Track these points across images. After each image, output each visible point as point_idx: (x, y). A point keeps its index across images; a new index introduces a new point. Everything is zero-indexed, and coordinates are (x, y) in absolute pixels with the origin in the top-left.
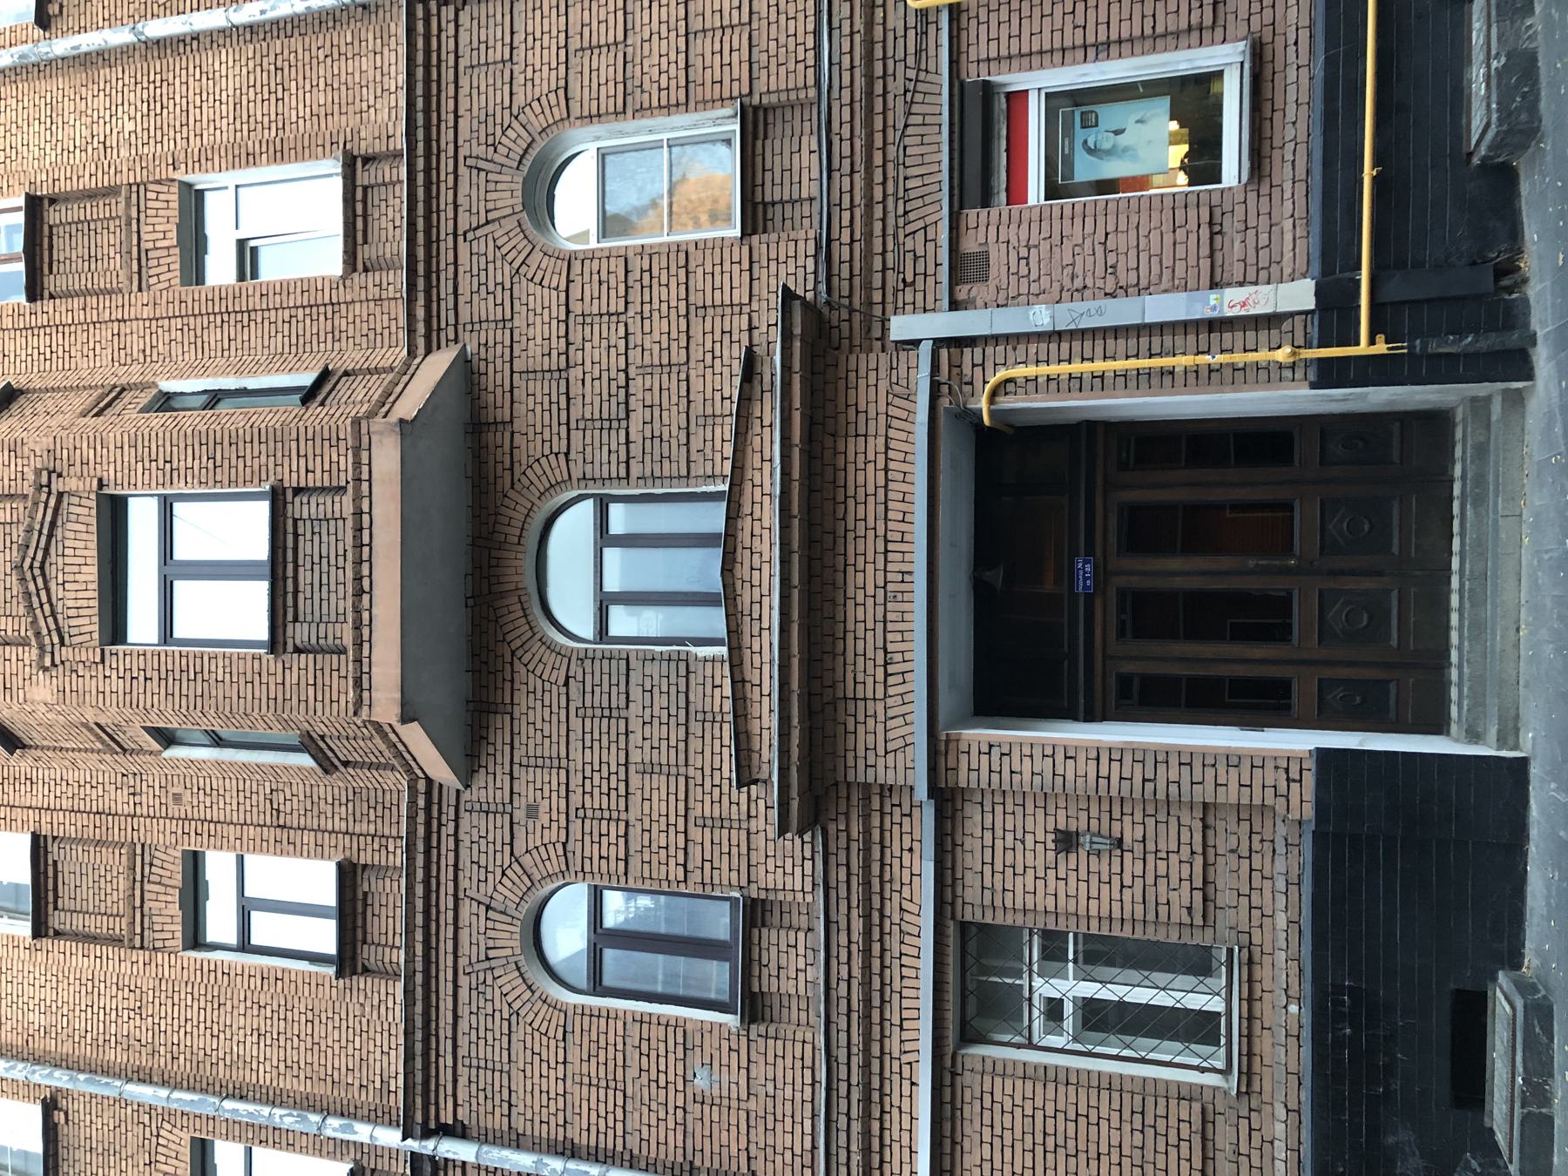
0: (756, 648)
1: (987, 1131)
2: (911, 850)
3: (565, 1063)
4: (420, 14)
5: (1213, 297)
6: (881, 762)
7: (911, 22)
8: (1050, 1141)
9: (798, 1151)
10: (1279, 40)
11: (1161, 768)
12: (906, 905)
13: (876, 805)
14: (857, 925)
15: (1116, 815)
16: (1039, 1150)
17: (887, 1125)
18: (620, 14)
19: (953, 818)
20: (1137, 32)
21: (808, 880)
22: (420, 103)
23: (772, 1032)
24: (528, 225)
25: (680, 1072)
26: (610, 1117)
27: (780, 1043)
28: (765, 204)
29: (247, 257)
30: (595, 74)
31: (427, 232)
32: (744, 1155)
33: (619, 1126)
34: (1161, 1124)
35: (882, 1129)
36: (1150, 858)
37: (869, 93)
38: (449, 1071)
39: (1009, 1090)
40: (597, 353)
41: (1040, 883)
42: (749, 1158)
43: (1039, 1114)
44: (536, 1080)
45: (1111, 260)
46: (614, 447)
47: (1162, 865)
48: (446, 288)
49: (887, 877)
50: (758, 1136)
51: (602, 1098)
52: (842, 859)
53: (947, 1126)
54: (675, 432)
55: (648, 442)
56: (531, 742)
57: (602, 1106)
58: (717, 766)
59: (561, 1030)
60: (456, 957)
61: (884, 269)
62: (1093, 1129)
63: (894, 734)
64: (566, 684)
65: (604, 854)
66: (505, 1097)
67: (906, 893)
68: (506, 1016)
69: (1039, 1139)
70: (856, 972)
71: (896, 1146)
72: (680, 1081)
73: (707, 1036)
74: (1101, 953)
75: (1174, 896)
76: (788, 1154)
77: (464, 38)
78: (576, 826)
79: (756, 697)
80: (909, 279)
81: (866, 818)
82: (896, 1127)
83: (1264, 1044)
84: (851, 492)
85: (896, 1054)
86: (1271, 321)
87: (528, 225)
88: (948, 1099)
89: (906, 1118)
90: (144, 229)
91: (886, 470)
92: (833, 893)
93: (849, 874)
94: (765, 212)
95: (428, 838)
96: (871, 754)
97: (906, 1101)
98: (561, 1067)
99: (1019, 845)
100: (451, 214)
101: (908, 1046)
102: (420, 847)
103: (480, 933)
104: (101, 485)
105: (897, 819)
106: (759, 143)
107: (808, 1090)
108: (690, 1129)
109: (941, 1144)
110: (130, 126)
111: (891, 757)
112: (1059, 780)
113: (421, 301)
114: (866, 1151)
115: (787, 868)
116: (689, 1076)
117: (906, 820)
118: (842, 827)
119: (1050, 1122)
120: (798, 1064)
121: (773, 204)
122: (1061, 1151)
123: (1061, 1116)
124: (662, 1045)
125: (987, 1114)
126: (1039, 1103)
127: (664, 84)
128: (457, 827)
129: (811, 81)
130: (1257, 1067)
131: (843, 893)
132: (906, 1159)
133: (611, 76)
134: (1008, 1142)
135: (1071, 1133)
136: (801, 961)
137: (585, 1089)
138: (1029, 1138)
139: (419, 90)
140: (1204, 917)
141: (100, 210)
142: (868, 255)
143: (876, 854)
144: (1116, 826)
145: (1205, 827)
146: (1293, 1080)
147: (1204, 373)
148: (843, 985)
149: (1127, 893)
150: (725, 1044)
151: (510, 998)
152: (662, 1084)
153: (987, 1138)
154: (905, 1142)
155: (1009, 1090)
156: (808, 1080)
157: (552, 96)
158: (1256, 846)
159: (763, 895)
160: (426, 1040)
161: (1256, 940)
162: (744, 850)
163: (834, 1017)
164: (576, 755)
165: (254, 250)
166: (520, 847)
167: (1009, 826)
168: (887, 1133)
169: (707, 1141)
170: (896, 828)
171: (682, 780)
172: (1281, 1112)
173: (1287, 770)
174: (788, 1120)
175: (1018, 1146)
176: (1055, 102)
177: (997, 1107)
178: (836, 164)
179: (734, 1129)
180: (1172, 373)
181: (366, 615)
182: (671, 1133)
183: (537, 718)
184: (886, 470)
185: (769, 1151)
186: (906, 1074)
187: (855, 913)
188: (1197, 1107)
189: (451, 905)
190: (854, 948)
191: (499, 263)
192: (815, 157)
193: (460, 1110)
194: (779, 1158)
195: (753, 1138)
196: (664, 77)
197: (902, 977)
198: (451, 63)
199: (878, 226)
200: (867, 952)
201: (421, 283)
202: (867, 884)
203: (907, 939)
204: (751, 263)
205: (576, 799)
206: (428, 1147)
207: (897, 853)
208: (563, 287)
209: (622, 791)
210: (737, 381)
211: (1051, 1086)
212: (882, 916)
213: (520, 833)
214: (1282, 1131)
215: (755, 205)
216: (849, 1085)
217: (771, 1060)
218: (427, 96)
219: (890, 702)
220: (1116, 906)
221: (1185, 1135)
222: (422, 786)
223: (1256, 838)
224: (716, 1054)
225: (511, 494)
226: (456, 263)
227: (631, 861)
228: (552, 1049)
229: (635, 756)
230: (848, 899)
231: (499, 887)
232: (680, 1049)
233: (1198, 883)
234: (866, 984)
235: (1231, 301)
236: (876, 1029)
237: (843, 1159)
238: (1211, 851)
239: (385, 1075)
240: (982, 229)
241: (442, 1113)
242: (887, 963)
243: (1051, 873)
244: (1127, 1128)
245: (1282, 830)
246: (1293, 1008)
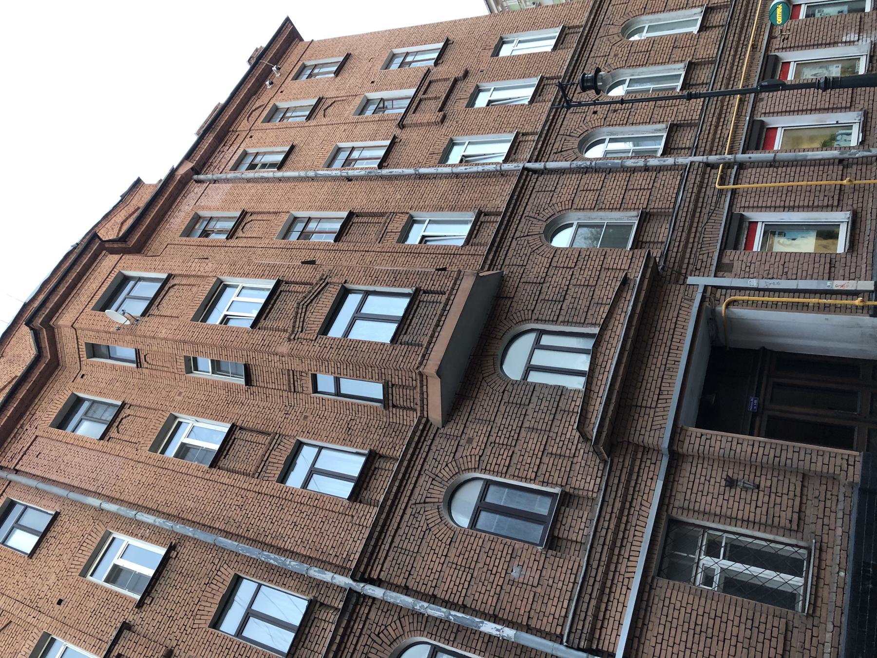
0: (600, 378)
1: (664, 618)
2: (652, 479)
3: (446, 556)
5: (829, 283)
6: (647, 434)
7: (716, 193)
8: (698, 628)
9: (557, 616)
10: (864, 213)
11: (784, 453)
12: (644, 503)
13: (639, 456)
14: (618, 505)
15: (758, 474)
16: (691, 632)
17: (609, 608)
19: (676, 468)
20: (806, 204)
21: (597, 486)
25: (505, 568)
26: (461, 586)
27: (562, 560)
31: (503, 235)
32: (526, 615)
33: (464, 591)
34: (762, 627)
35: (606, 609)
36: (773, 496)
37: (695, 211)
38: (385, 552)
39: (680, 598)
40: (558, 279)
41: (714, 501)
42: (529, 618)
43: (694, 613)
44: (428, 563)
45: (786, 270)
47: (778, 500)
49: (637, 489)
50: (537, 606)
51: (460, 576)
52: (618, 474)
53: (642, 613)
56: (479, 412)
57: (458, 580)
58: (565, 432)
59: (450, 540)
60: (409, 500)
61: (688, 264)
62: (723, 625)
63: (658, 425)
64: (503, 392)
65: (498, 462)
66: (409, 569)
67: (645, 497)
68: (424, 529)
69: (692, 626)
70: (612, 526)
71: (612, 620)
72: (504, 572)
73: (525, 551)
74: (737, 553)
75: (783, 514)
76: (551, 617)
78: (489, 449)
80: (698, 267)
81: (634, 460)
82: (614, 609)
83: (824, 592)
84: (658, 329)
85: (622, 572)
86: (855, 294)
88: (645, 599)
89: (620, 605)
91: (676, 323)
92: (609, 489)
93: (619, 481)
95: (417, 443)
96: (643, 430)
97: (622, 597)
98: (443, 558)
99: (707, 483)
101: (630, 569)
102: (413, 445)
103: (428, 488)
104: (345, 282)
105: (648, 464)
107: (571, 585)
108: (501, 598)
109: (636, 622)
110: (399, 197)
111: (652, 432)
112: (732, 452)
113: (492, 254)
114: (596, 617)
115: (588, 478)
116: (509, 571)
117: (652, 466)
118: (621, 460)
119: (700, 618)
120: (569, 572)
122: (703, 634)
123: (706, 615)
124: (500, 553)
125: (665, 609)
126: (695, 607)
128: (431, 443)
129: (672, 206)
130: (819, 603)
131: (614, 489)
132: (616, 627)
134: (674, 625)
135: (711, 625)
136: (583, 525)
137: (452, 570)
138: (686, 625)
139: (517, 193)
140: (798, 526)
142: (683, 257)
143: (634, 477)
144: (757, 479)
145: (803, 486)
146: (839, 610)
147: (822, 307)
148: (604, 531)
149: (758, 510)
150: (533, 557)
151: (429, 522)
152: (494, 572)
153: (663, 622)
154: (617, 618)
155: (680, 598)
156: (572, 580)
158: (829, 496)
159: (572, 491)
160: (380, 533)
161: (825, 540)
162: (568, 469)
163: (595, 546)
164: (498, 420)
166: (458, 455)
167: (704, 473)
168: (608, 612)
169: (509, 604)
170: (647, 469)
172: (830, 627)
173: (847, 460)
174: (556, 599)
175: (680, 628)
176: (768, 228)
177: (672, 606)
178: (677, 228)
179: (525, 600)
180: (808, 306)
181: (437, 334)
182: (491, 598)
183: (486, 403)
184: (676, 323)
185: (541, 614)
186: (626, 582)
187: (618, 499)
188: (783, 621)
189: (416, 475)
190: (614, 515)
192: (667, 230)
193: (382, 573)
194: (545, 619)
195: (534, 607)
197: (634, 536)
199: (689, 250)
200: (619, 519)
201: (494, 249)
202: (627, 489)
203: (641, 518)
205: (492, 439)
206: (359, 587)
207: (645, 479)
209: (515, 438)
210: (618, 284)
211: (703, 600)
212: (631, 506)
213: (461, 449)
214: (830, 634)
215: (638, 241)
216: (595, 581)
217: (555, 568)
219: (657, 410)
220: (752, 515)
221: (775, 635)
222: (424, 420)
223: (829, 493)
224: (527, 561)
225: (505, 322)
227: (510, 468)
228: (442, 548)
230: (617, 491)
231: (443, 471)
232: (509, 556)
233: (797, 509)
234: (615, 533)
235: (837, 284)
236: (615, 558)
237: (582, 617)
238: (805, 498)
239: (350, 551)
240: (730, 255)
241: (373, 572)
242: (628, 528)
243: (721, 497)
244: (743, 626)
245: (843, 490)
246: (842, 574)
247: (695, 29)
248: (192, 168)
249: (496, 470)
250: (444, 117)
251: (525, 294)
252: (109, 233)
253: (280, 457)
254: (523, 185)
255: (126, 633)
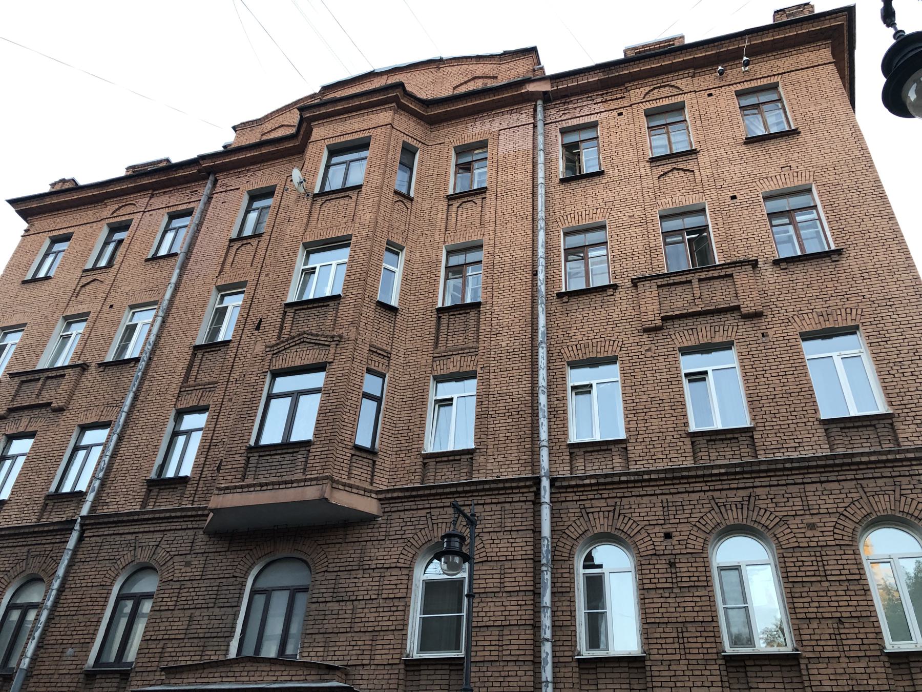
0: (216, 675)
4: (528, 483)
18: (517, 588)
22: (487, 486)
23: (80, 685)
24: (429, 545)
28: (908, 663)
29: (584, 390)
30: (491, 576)
40: (366, 584)
46: (325, 595)
48: (407, 505)
54: (326, 626)
55: (323, 613)
64: (234, 577)
77: (518, 505)
79: (197, 676)
87: (429, 545)
90: (459, 356)
94: (740, 666)
100: (439, 505)
102: (183, 514)
106: (447, 667)
110: (504, 344)
113: (400, 494)
116: (73, 646)
121: (746, 672)
127: (480, 614)
133: (489, 585)
141: (471, 335)
157: (484, 554)
165: (704, 379)
171: (182, 636)
191: (413, 531)
196: (484, 614)
198: (507, 500)
201: (407, 494)
204: (392, 664)
206: (77, 527)
208: (399, 565)
218: (490, 489)
226: (417, 509)
229: (197, 613)
247: (892, 646)
248: (545, 93)
249: (644, 572)
250: (656, 329)
251: (349, 554)
252: (423, 87)
253: (453, 366)
254: (512, 488)
255: (749, 268)
